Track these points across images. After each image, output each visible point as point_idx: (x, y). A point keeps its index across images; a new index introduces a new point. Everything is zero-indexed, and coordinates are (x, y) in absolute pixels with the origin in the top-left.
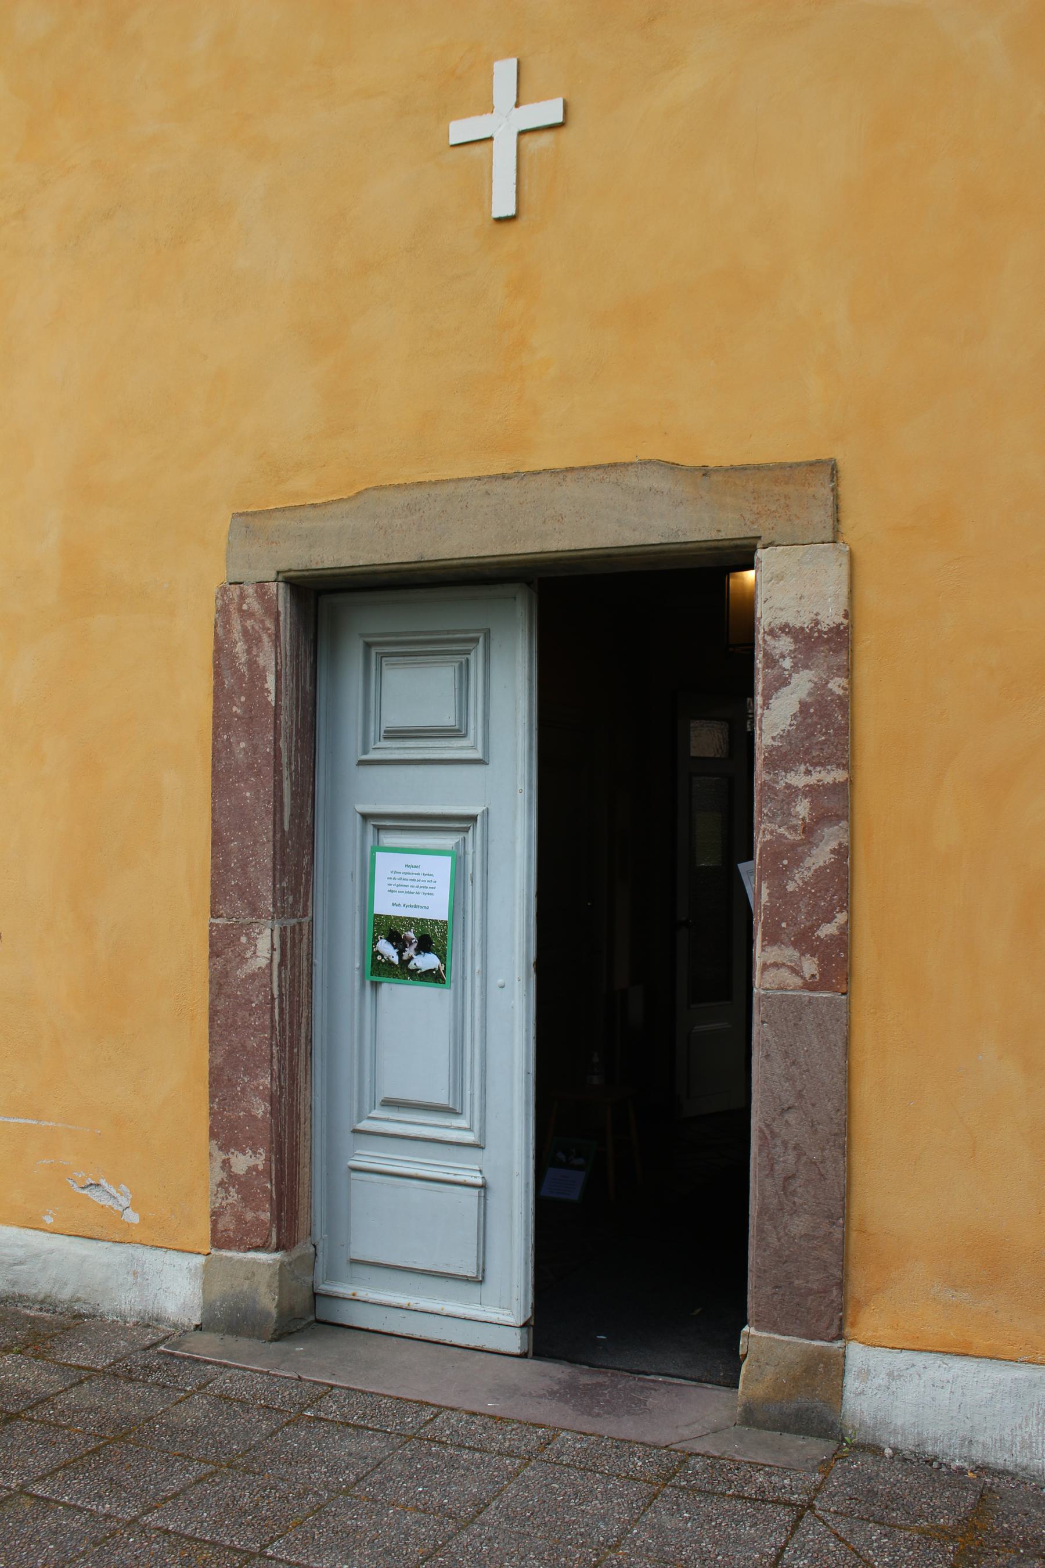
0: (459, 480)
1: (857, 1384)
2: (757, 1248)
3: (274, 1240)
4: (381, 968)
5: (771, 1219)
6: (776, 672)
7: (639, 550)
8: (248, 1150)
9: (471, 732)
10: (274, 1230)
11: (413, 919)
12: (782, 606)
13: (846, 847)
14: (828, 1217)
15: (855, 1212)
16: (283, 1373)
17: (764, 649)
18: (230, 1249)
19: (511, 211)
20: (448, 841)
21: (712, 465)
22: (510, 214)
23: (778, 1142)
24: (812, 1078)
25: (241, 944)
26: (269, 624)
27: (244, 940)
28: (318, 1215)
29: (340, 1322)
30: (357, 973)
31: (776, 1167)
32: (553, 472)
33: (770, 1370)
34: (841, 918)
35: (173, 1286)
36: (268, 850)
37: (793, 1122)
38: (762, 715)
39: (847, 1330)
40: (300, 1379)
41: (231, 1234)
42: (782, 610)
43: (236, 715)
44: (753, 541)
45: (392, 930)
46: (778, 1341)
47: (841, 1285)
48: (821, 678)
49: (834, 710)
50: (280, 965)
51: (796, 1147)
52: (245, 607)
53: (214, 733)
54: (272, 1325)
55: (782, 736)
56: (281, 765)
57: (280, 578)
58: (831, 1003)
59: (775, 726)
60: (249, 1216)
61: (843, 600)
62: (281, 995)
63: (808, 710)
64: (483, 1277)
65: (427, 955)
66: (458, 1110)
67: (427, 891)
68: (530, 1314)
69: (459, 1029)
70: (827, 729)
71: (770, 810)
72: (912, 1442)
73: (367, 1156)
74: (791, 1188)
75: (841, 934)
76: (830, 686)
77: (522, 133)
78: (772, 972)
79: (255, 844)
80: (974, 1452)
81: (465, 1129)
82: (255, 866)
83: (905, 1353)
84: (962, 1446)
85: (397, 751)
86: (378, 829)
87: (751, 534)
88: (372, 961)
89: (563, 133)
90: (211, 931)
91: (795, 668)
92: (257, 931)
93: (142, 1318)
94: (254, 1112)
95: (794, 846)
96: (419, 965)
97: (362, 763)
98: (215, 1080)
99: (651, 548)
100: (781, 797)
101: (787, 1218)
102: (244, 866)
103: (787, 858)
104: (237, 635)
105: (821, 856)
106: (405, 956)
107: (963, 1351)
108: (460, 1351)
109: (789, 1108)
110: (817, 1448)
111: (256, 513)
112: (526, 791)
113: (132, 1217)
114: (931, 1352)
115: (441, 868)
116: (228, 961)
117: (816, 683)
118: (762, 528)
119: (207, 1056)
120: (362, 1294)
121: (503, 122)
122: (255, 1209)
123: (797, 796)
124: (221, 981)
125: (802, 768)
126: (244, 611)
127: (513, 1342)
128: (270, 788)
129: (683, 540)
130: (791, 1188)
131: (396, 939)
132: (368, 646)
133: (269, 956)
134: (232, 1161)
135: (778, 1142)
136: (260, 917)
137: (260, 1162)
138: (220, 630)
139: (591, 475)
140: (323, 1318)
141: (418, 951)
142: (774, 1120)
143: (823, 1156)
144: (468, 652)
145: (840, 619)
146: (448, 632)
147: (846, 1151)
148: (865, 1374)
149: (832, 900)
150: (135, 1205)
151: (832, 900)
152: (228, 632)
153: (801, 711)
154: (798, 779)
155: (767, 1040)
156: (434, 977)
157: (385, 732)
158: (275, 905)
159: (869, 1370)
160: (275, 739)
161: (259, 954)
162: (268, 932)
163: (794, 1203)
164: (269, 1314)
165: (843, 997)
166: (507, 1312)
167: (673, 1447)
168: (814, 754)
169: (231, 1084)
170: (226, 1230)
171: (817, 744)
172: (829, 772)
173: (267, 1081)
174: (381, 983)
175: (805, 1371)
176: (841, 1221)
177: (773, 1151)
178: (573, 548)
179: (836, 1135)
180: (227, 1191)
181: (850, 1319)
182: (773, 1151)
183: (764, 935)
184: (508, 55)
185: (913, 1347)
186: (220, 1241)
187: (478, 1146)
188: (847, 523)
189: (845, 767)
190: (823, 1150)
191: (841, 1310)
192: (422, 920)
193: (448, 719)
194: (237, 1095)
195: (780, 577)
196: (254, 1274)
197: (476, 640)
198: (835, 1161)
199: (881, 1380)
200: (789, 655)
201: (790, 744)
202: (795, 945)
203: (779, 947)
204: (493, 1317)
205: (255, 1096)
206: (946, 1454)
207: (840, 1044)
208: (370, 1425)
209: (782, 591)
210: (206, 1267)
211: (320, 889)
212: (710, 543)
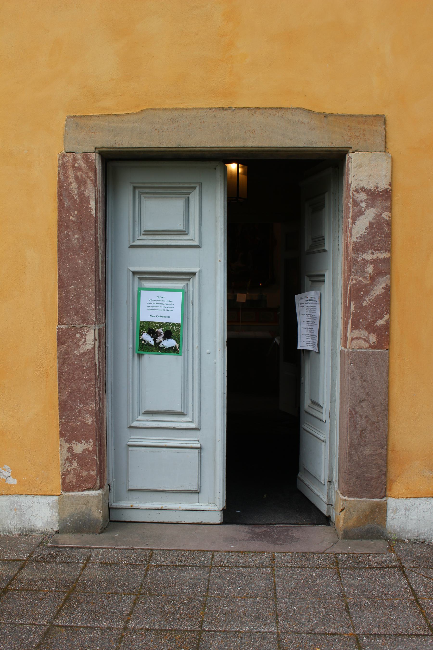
0: (199, 108)
1: (392, 515)
2: (348, 462)
3: (98, 484)
4: (144, 347)
5: (355, 449)
6: (358, 208)
8: (83, 441)
9: (191, 232)
11: (162, 323)
12: (362, 179)
13: (389, 286)
14: (380, 446)
15: (391, 443)
16: (123, 547)
17: (353, 198)
18: (73, 491)
20: (180, 285)
21: (328, 112)
23: (358, 415)
24: (373, 386)
27: (78, 335)
28: (111, 470)
30: (131, 350)
31: (357, 426)
32: (249, 109)
34: (386, 317)
35: (42, 513)
36: (92, 289)
38: (351, 228)
39: (388, 493)
40: (133, 549)
41: (74, 484)
42: (361, 181)
43: (72, 221)
44: (347, 149)
46: (358, 501)
47: (385, 474)
48: (379, 212)
49: (384, 226)
50: (99, 347)
51: (366, 417)
52: (76, 165)
54: (100, 526)
55: (361, 237)
57: (97, 151)
58: (381, 354)
59: (358, 232)
60: (84, 473)
61: (389, 178)
62: (99, 362)
63: (373, 226)
64: (200, 490)
65: (169, 340)
66: (185, 413)
67: (169, 309)
68: (225, 504)
69: (186, 375)
72: (415, 535)
73: (137, 439)
74: (364, 435)
75: (387, 324)
76: (383, 215)
79: (84, 287)
81: (190, 422)
82: (85, 298)
83: (412, 499)
85: (151, 241)
86: (140, 279)
87: (347, 146)
90: (58, 332)
91: (367, 207)
92: (86, 331)
94: (86, 422)
95: (366, 286)
96: (165, 345)
97: (132, 246)
98: (62, 407)
101: (362, 448)
102: (78, 298)
103: (363, 291)
104: (71, 179)
105: (378, 290)
106: (158, 341)
108: (190, 525)
109: (363, 400)
111: (82, 116)
113: (13, 481)
114: (422, 497)
116: (69, 347)
117: (376, 214)
118: (353, 143)
119: (57, 395)
120: (136, 505)
122: (88, 470)
123: (367, 264)
124: (65, 357)
125: (370, 251)
126: (76, 167)
127: (218, 518)
128: (93, 258)
129: (315, 146)
130: (364, 435)
131: (152, 333)
132: (135, 188)
133: (93, 343)
134: (73, 448)
136: (88, 324)
137: (90, 446)
138: (62, 177)
139: (269, 112)
140: (114, 519)
141: (164, 338)
142: (356, 406)
143: (378, 420)
144: (189, 194)
145: (387, 186)
146: (180, 183)
147: (387, 416)
148: (395, 510)
149: (382, 309)
150: (13, 475)
151: (382, 309)
153: (370, 226)
154: (368, 256)
156: (173, 350)
157: (144, 231)
158: (96, 318)
159: (397, 509)
160: (95, 233)
161: (87, 342)
163: (365, 441)
164: (98, 520)
165: (387, 351)
166: (213, 505)
167: (326, 552)
169: (72, 409)
171: (376, 241)
172: (382, 253)
173: (94, 406)
174: (143, 354)
175: (370, 512)
176: (386, 447)
177: (356, 420)
178: (260, 146)
179: (384, 410)
180: (71, 462)
181: (388, 488)
182: (356, 420)
183: (352, 325)
185: (415, 496)
186: (66, 488)
187: (198, 430)
188: (390, 144)
190: (378, 417)
192: (167, 323)
193: (180, 226)
194: (76, 414)
196: (88, 502)
197: (194, 188)
198: (384, 422)
199: (402, 512)
200: (364, 201)
201: (365, 241)
202: (366, 329)
203: (359, 330)
204: (207, 508)
205: (86, 414)
207: (385, 371)
208: (187, 564)
209: (362, 172)
210: (60, 502)
211: (110, 309)
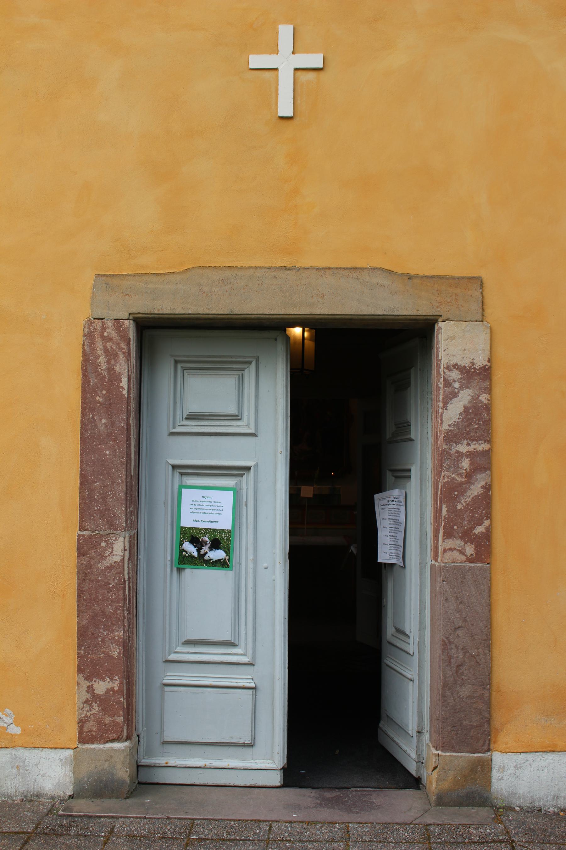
1: (498, 775)
2: (442, 706)
4: (185, 560)
5: (450, 689)
6: (450, 389)
7: (370, 317)
8: (107, 678)
10: (125, 727)
11: (208, 529)
12: (454, 354)
13: (490, 485)
15: (495, 681)
17: (444, 377)
18: (93, 743)
19: (291, 114)
20: (231, 482)
21: (413, 273)
22: (290, 115)
23: (453, 646)
25: (102, 547)
26: (123, 345)
27: (103, 544)
28: (141, 716)
29: (153, 782)
31: (452, 660)
32: (317, 269)
33: (451, 773)
34: (487, 523)
35: (51, 772)
36: (122, 487)
37: (461, 635)
38: (442, 413)
39: (492, 746)
40: (168, 818)
41: (94, 733)
43: (99, 402)
44: (437, 317)
45: (194, 537)
47: (489, 721)
48: (475, 394)
49: (482, 411)
51: (463, 649)
52: (105, 334)
53: (82, 413)
55: (454, 425)
56: (130, 434)
57: (131, 317)
58: (481, 569)
59: (450, 419)
60: (108, 720)
61: (487, 352)
62: (129, 578)
66: (236, 644)
68: (286, 761)
69: (237, 595)
70: (479, 421)
71: (447, 465)
72: (528, 802)
73: (175, 676)
74: (461, 671)
76: (480, 398)
77: (296, 70)
78: (449, 553)
79: (112, 484)
80: (559, 802)
81: (241, 655)
83: (523, 755)
84: (553, 800)
85: (195, 427)
86: (182, 474)
88: (180, 555)
89: (322, 74)
90: (78, 540)
91: (461, 388)
92: (114, 539)
93: (26, 796)
94: (111, 654)
95: (461, 484)
96: (211, 557)
99: (377, 317)
100: (453, 457)
101: (458, 688)
102: (104, 498)
104: (99, 351)
105: (476, 489)
106: (202, 552)
107: (553, 749)
109: (459, 627)
110: (484, 813)
111: (113, 275)
112: (284, 452)
113: (16, 730)
114: (536, 752)
115: (226, 499)
117: (472, 397)
118: (443, 310)
119: (75, 620)
120: (172, 762)
121: (285, 61)
122: (112, 716)
123: (463, 457)
124: (86, 572)
125: (465, 442)
126: (105, 337)
127: (276, 779)
128: (124, 448)
130: (461, 671)
131: (196, 541)
132: (176, 362)
133: (122, 554)
134: (94, 686)
135: (453, 646)
136: (116, 530)
137: (116, 685)
141: (211, 549)
142: (450, 634)
143: (478, 652)
144: (243, 370)
145: (485, 363)
146: (232, 357)
147: (489, 648)
148: (502, 769)
149: (482, 513)
150: (17, 722)
151: (482, 513)
152: (93, 349)
153: (465, 411)
154: (463, 448)
155: (446, 591)
156: (222, 564)
157: (187, 415)
158: (126, 523)
159: (504, 766)
160: (127, 418)
161: (114, 553)
162: (121, 539)
163: (462, 679)
164: (124, 781)
166: (270, 762)
168: (472, 434)
169: (94, 637)
170: (89, 731)
171: (473, 429)
172: (480, 444)
173: (121, 634)
174: (184, 569)
175: (470, 771)
176: (488, 687)
177: (450, 652)
178: (330, 313)
179: (485, 640)
180: (91, 706)
181: (493, 740)
182: (450, 652)
183: (444, 533)
184: (288, 22)
185: (527, 750)
186: (84, 738)
187: (251, 664)
188: (488, 311)
189: (489, 442)
190: (478, 649)
191: (489, 735)
193: (231, 409)
194: (98, 644)
195: (452, 338)
196: (112, 757)
197: (250, 363)
198: (485, 655)
200: (458, 380)
201: (458, 429)
202: (462, 538)
204: (263, 766)
205: (112, 643)
206: (546, 805)
207: (486, 591)
208: (238, 838)
209: (454, 345)
210: (75, 757)
212: (412, 317)
